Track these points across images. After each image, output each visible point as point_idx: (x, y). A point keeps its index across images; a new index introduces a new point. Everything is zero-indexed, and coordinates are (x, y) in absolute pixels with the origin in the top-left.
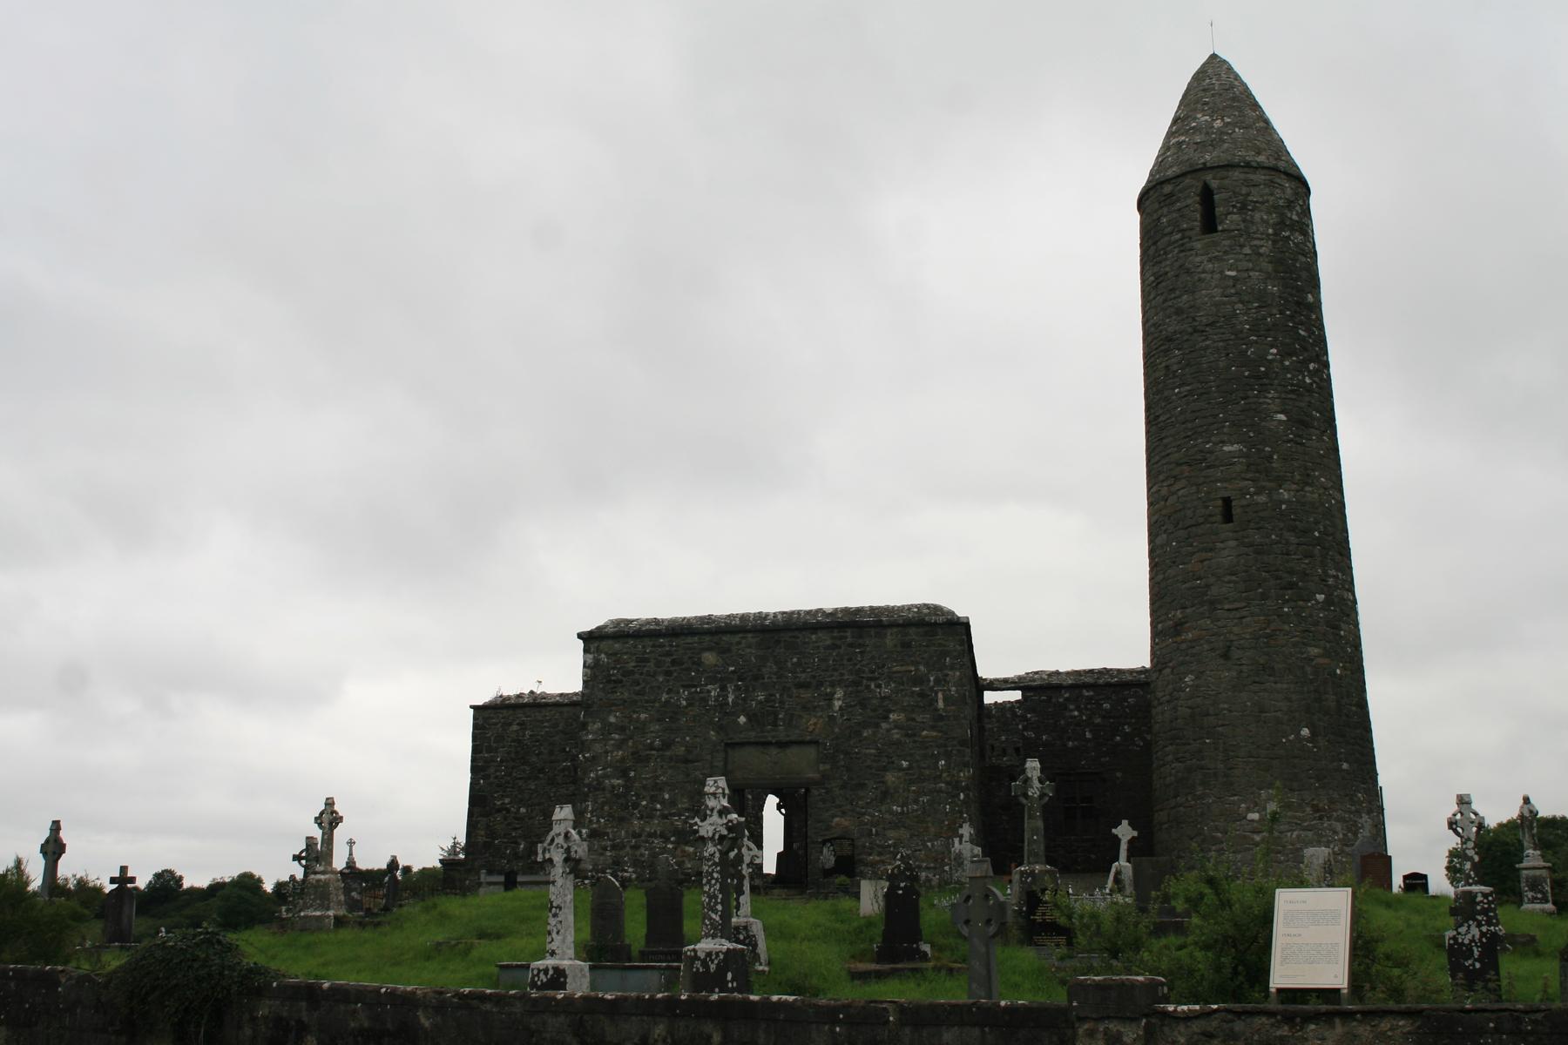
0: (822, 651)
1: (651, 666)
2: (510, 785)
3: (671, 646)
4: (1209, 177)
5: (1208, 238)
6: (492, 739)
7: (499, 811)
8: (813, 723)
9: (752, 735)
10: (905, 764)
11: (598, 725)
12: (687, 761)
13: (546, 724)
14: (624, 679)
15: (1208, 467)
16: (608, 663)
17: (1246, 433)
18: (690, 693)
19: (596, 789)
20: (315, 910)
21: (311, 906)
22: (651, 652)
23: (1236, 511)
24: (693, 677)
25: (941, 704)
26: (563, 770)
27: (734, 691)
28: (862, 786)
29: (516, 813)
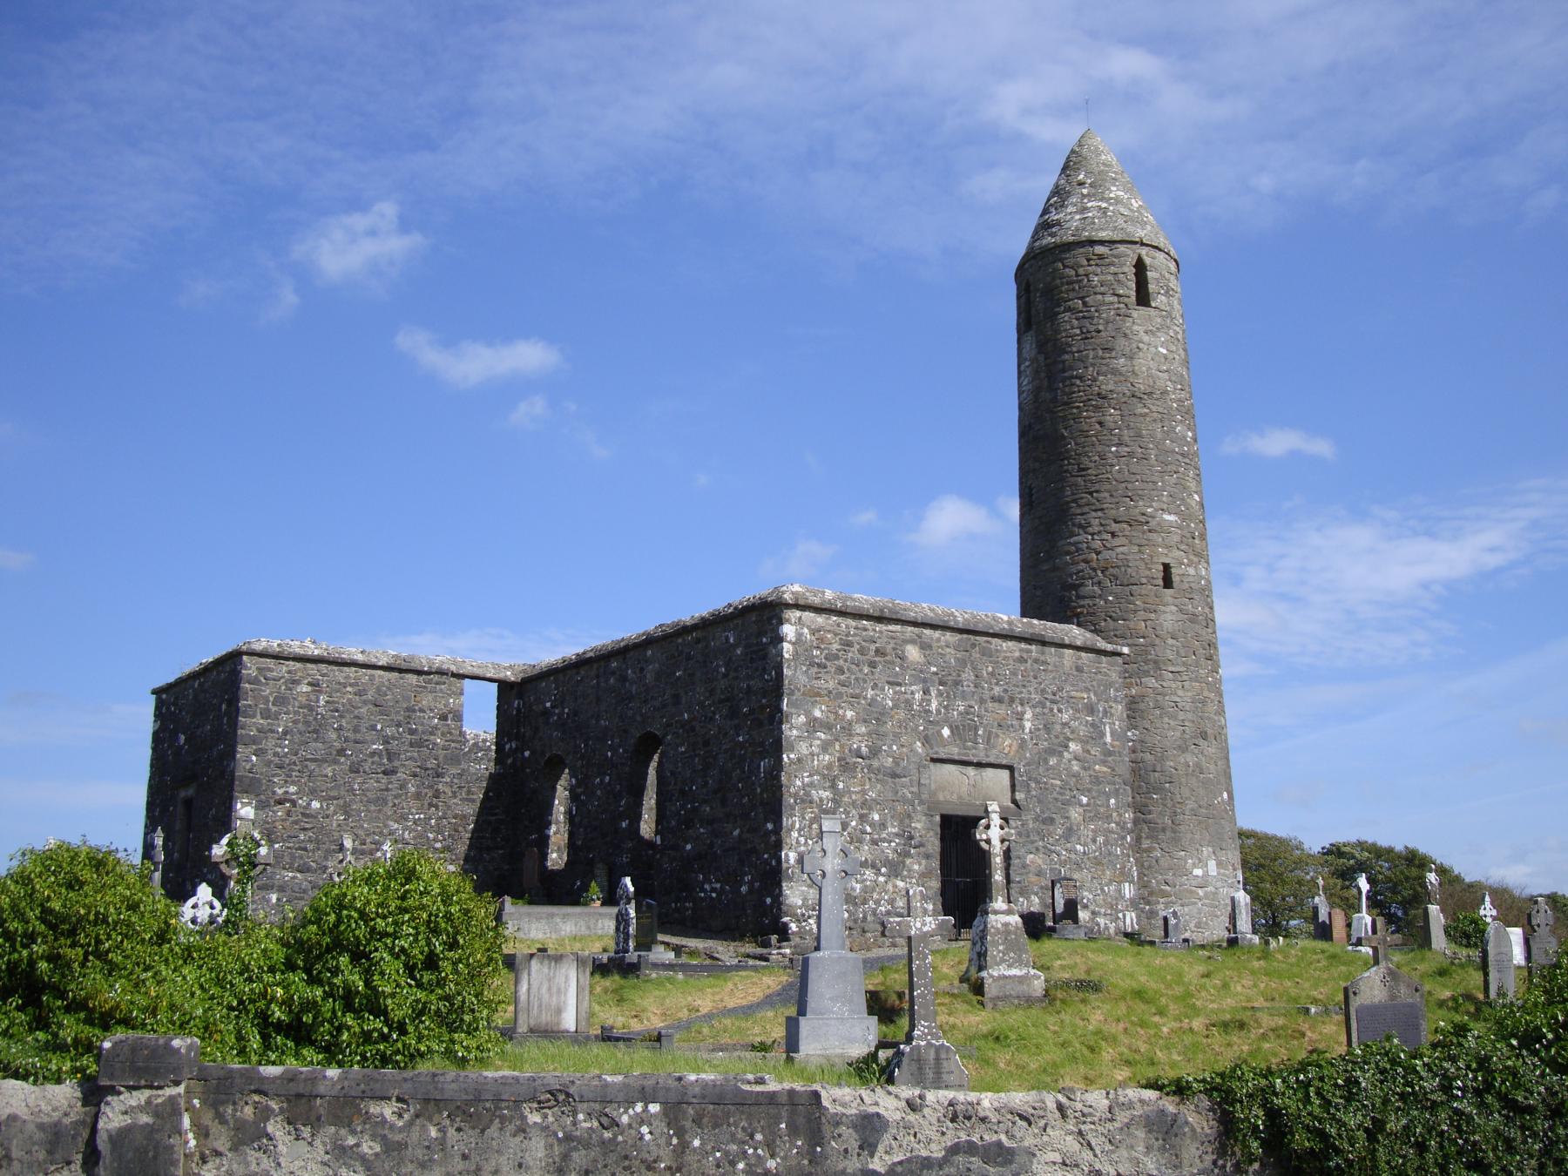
0: (1012, 663)
1: (853, 653)
2: (297, 768)
3: (875, 630)
4: (1144, 251)
5: (1143, 310)
6: (271, 699)
7: (280, 802)
8: (1006, 746)
9: (954, 752)
10: (1085, 800)
11: (802, 719)
12: (894, 776)
13: (349, 689)
14: (828, 664)
15: (1150, 531)
16: (811, 641)
17: (1179, 506)
18: (895, 693)
19: (803, 801)
20: (1010, 966)
21: (1002, 960)
22: (855, 635)
23: (1175, 579)
24: (897, 673)
25: (1108, 739)
26: (373, 754)
27: (936, 697)
28: (1052, 821)
29: (305, 808)
